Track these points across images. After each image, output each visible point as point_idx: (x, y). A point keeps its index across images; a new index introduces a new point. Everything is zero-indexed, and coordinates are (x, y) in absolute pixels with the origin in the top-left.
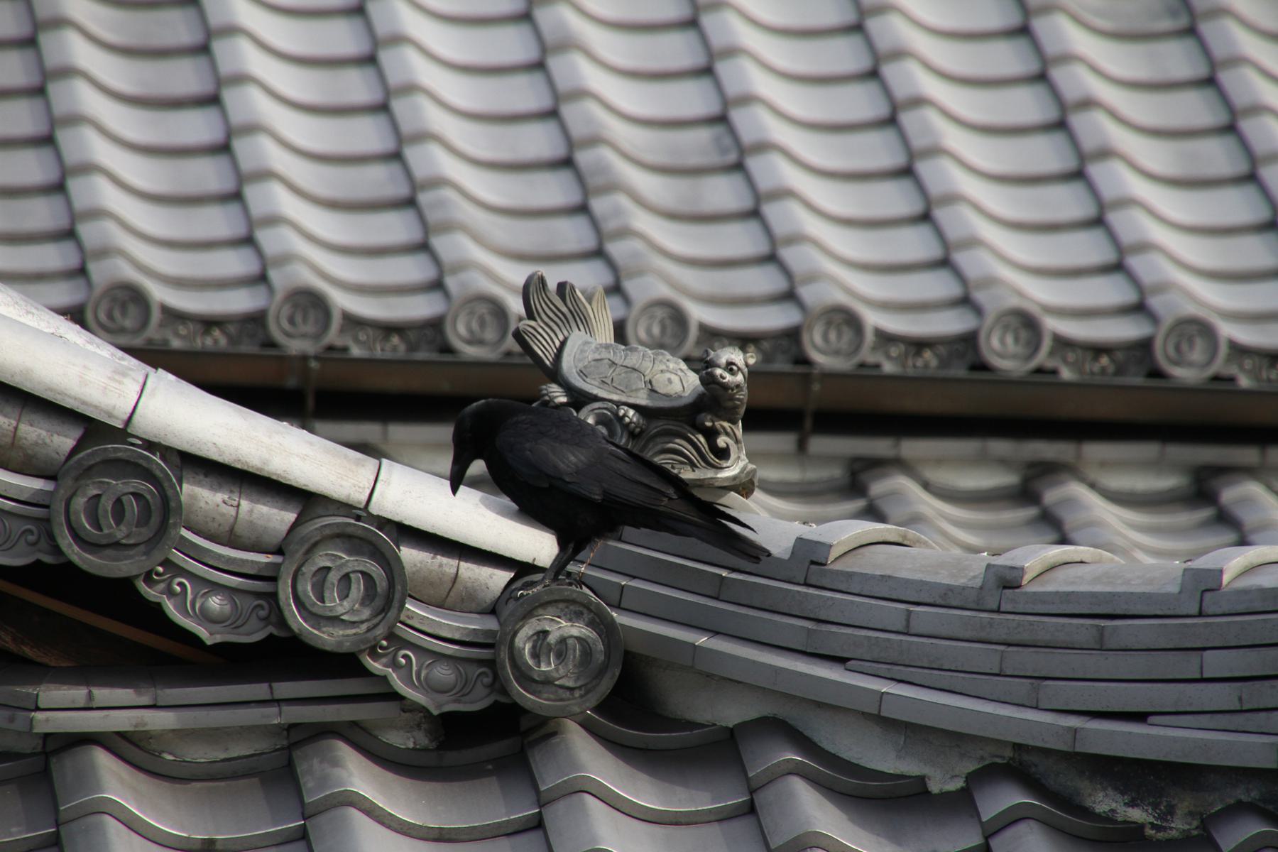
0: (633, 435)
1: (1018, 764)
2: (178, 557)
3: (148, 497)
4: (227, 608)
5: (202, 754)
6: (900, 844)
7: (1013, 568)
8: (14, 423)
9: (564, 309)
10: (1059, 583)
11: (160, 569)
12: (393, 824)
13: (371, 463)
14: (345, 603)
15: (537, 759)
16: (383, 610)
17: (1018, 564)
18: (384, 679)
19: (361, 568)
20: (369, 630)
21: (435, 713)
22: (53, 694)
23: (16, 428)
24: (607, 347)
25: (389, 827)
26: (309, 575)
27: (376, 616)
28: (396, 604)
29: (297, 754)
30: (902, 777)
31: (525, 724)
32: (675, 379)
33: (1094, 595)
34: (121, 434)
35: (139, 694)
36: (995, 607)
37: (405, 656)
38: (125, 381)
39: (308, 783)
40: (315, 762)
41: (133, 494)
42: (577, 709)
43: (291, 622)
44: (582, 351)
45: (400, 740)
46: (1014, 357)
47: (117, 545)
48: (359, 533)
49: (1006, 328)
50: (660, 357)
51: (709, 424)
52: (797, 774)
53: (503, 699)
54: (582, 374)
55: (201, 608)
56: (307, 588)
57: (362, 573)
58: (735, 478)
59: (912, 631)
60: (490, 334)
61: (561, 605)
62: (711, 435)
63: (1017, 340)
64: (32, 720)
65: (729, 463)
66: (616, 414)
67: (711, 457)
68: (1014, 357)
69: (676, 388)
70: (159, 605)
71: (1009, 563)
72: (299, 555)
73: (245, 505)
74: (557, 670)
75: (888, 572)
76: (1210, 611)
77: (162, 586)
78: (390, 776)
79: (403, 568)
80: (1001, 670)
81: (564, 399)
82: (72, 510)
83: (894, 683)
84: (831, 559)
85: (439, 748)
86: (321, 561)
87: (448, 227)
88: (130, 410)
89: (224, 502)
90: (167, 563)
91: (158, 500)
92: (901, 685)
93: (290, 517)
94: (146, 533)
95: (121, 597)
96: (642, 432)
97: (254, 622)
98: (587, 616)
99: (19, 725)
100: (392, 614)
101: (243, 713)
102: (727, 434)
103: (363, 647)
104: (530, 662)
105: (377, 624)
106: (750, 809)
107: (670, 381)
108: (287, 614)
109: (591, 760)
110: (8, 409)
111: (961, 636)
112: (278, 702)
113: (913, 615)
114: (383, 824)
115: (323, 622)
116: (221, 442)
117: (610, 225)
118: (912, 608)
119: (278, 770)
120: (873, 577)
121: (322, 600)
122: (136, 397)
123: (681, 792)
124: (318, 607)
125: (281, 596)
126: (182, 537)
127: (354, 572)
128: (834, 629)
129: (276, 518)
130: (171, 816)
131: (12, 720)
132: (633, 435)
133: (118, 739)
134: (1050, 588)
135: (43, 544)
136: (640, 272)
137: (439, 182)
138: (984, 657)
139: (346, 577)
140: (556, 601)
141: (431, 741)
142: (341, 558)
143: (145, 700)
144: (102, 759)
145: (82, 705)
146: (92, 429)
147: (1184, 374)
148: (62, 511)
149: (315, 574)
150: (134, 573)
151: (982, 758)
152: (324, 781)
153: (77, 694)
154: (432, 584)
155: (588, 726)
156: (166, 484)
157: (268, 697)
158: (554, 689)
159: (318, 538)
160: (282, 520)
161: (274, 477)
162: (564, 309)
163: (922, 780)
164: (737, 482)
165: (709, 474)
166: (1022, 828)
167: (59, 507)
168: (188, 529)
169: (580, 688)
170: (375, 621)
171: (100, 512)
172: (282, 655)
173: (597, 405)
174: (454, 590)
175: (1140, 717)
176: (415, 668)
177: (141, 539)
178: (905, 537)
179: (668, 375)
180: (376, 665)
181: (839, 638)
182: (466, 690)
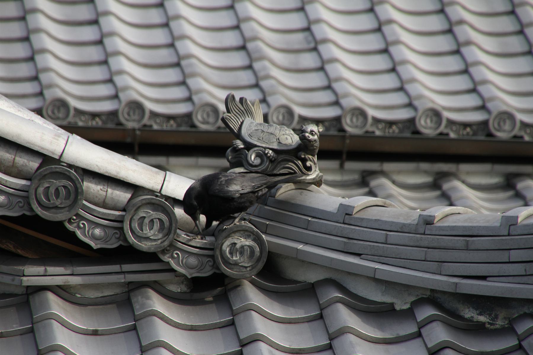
0: (271, 161)
1: (432, 297)
2: (82, 212)
3: (69, 187)
4: (103, 234)
5: (92, 294)
7: (430, 216)
8: (13, 157)
9: (242, 109)
10: (450, 222)
11: (75, 218)
12: (172, 323)
13: (162, 173)
14: (152, 231)
15: (232, 296)
17: (432, 214)
18: (168, 263)
19: (158, 217)
20: (161, 243)
21: (189, 277)
22: (30, 269)
23: (14, 159)
24: (261, 124)
25: (170, 325)
26: (136, 220)
28: (173, 232)
29: (132, 294)
30: (384, 303)
31: (227, 281)
32: (289, 138)
33: (464, 227)
34: (58, 161)
35: (66, 270)
36: (423, 232)
37: (176, 254)
38: (60, 139)
39: (136, 306)
40: (140, 298)
41: (63, 186)
42: (248, 275)
43: (129, 240)
44: (250, 126)
45: (175, 288)
46: (431, 128)
47: (56, 207)
48: (157, 202)
49: (427, 116)
50: (283, 129)
51: (303, 156)
53: (217, 271)
54: (250, 136)
55: (91, 234)
56: (135, 225)
57: (159, 219)
58: (314, 179)
59: (388, 242)
60: (211, 120)
61: (242, 232)
62: (304, 161)
63: (431, 121)
64: (21, 280)
65: (311, 173)
66: (264, 153)
68: (431, 128)
69: (289, 141)
70: (74, 232)
71: (429, 214)
72: (132, 212)
73: (110, 191)
74: (240, 259)
75: (378, 218)
76: (513, 234)
77: (75, 225)
81: (242, 146)
82: (38, 193)
83: (380, 264)
84: (354, 212)
85: (191, 292)
87: (194, 75)
88: (61, 151)
89: (101, 190)
90: (77, 215)
93: (128, 196)
94: (68, 202)
95: (58, 229)
96: (275, 160)
97: (113, 240)
98: (252, 237)
99: (16, 282)
100: (171, 236)
102: (311, 161)
103: (159, 250)
104: (229, 256)
107: (287, 138)
108: (127, 236)
109: (254, 296)
110: (11, 151)
113: (389, 236)
114: (168, 323)
115: (142, 240)
116: (99, 164)
117: (261, 74)
119: (124, 300)
120: (371, 220)
122: (64, 146)
123: (292, 310)
124: (140, 233)
125: (125, 229)
126: (84, 204)
128: (355, 242)
129: (123, 196)
131: (13, 280)
133: (58, 288)
135: (26, 207)
136: (274, 93)
137: (190, 56)
138: (419, 253)
141: (188, 289)
143: (68, 272)
144: (51, 297)
146: (46, 159)
147: (501, 135)
150: (64, 219)
152: (143, 305)
153: (40, 269)
155: (253, 282)
156: (77, 182)
157: (120, 271)
158: (238, 267)
159: (140, 205)
160: (125, 197)
161: (122, 179)
162: (242, 109)
163: (392, 304)
164: (315, 181)
166: (434, 324)
169: (249, 267)
171: (49, 194)
172: (125, 253)
173: (256, 149)
175: (483, 278)
176: (181, 259)
177: (66, 205)
178: (385, 203)
179: (286, 136)
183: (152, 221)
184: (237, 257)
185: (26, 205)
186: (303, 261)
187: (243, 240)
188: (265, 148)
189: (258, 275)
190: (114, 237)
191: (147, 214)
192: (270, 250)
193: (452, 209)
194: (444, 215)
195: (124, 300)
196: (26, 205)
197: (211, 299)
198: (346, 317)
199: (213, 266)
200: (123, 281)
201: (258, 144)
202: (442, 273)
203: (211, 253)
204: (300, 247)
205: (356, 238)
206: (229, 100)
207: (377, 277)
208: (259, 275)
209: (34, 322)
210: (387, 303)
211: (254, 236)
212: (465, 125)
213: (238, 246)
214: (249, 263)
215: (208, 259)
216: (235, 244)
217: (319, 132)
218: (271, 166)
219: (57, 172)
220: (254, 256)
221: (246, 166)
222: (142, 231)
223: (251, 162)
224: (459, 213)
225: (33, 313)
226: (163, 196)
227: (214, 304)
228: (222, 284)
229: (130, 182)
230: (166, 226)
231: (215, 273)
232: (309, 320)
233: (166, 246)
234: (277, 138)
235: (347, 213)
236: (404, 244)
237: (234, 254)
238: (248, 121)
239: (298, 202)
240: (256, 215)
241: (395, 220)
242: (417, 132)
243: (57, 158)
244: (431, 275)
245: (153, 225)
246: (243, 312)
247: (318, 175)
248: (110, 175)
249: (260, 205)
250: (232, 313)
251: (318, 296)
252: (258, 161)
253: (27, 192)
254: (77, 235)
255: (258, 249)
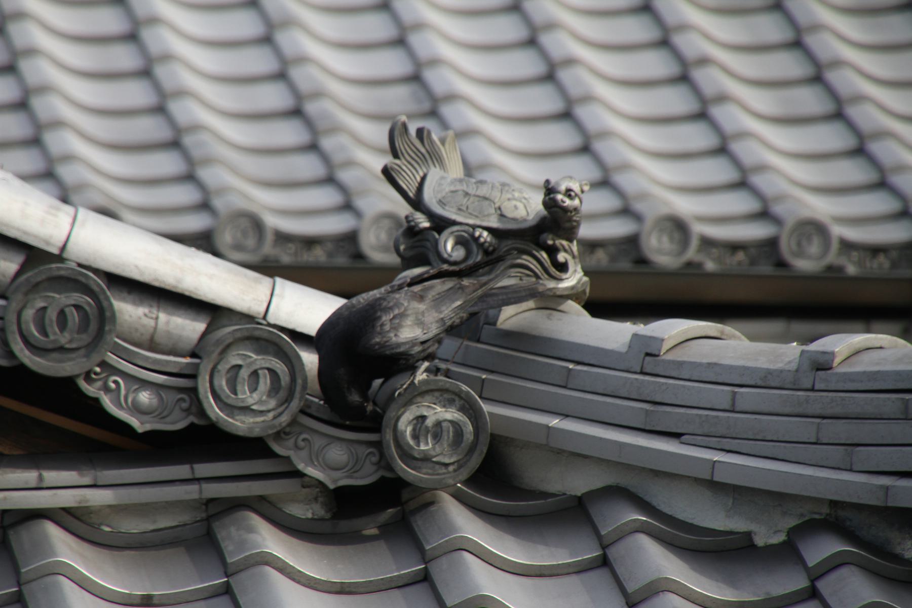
1: (835, 518)
2: (112, 359)
3: (87, 308)
4: (155, 401)
5: (134, 526)
7: (824, 353)
9: (423, 150)
11: (98, 369)
12: (302, 580)
13: (266, 281)
15: (419, 523)
16: (286, 401)
17: (828, 349)
20: (275, 418)
21: (332, 487)
24: (461, 181)
25: (298, 582)
26: (223, 372)
27: (282, 404)
29: (216, 525)
31: (405, 495)
33: (898, 373)
35: (82, 475)
39: (228, 547)
42: (451, 482)
44: (440, 185)
45: (301, 511)
47: (61, 349)
48: (265, 335)
51: (550, 242)
53: (388, 475)
54: (441, 203)
56: (222, 383)
57: (269, 369)
58: (573, 288)
59: (738, 409)
60: (251, 242)
61: (437, 394)
62: (552, 251)
65: (568, 275)
66: (472, 236)
67: (553, 270)
69: (521, 213)
70: (97, 400)
71: (821, 349)
72: (215, 356)
73: (163, 317)
74: (434, 448)
78: (294, 541)
80: (818, 439)
81: (426, 224)
83: (723, 453)
86: (234, 359)
87: (209, 161)
88: (64, 238)
89: (145, 315)
90: (103, 364)
92: (730, 455)
94: (86, 338)
95: (64, 395)
96: (494, 250)
97: (177, 414)
98: (458, 402)
101: (170, 488)
102: (566, 251)
103: (270, 432)
104: (412, 442)
106: (604, 562)
107: (516, 207)
108: (205, 405)
111: (780, 411)
112: (198, 480)
113: (738, 396)
114: (293, 580)
115: (236, 412)
117: (337, 158)
118: (737, 389)
119: (201, 535)
124: (231, 399)
125: (201, 390)
126: (116, 343)
127: (262, 368)
129: (190, 328)
133: (64, 514)
134: (859, 368)
137: (196, 128)
140: (432, 391)
141: (327, 512)
142: (250, 357)
143: (87, 480)
144: (53, 531)
145: (33, 485)
147: (804, 265)
150: (76, 372)
151: (802, 515)
152: (242, 545)
153: (29, 476)
155: (459, 497)
156: (102, 297)
157: (189, 476)
158: (431, 465)
159: (231, 340)
161: (187, 293)
162: (423, 150)
163: (748, 535)
165: (551, 284)
166: (844, 571)
178: (722, 332)
179: (514, 202)
181: (671, 418)
183: (255, 374)
184: (427, 444)
186: (560, 452)
187: (439, 409)
189: (468, 482)
190: (177, 408)
191: (244, 360)
192: (496, 432)
193: (868, 339)
194: (852, 351)
195: (201, 535)
197: (374, 531)
198: (656, 560)
199: (378, 463)
201: (459, 219)
202: (855, 468)
204: (555, 422)
205: (669, 402)
206: (396, 133)
207: (715, 479)
209: (22, 581)
211: (462, 402)
212: (734, 247)
214: (451, 456)
215: (371, 450)
216: (423, 418)
220: (462, 442)
222: (236, 394)
223: (445, 256)
224: (881, 348)
225: (20, 563)
226: (269, 325)
230: (283, 383)
233: (284, 425)
234: (497, 205)
235: (649, 351)
236: (771, 410)
237: (422, 439)
238: (434, 174)
239: (546, 334)
240: (459, 361)
242: (642, 261)
243: (56, 251)
247: (580, 280)
249: (466, 343)
251: (595, 520)
252: (459, 254)
254: (104, 404)
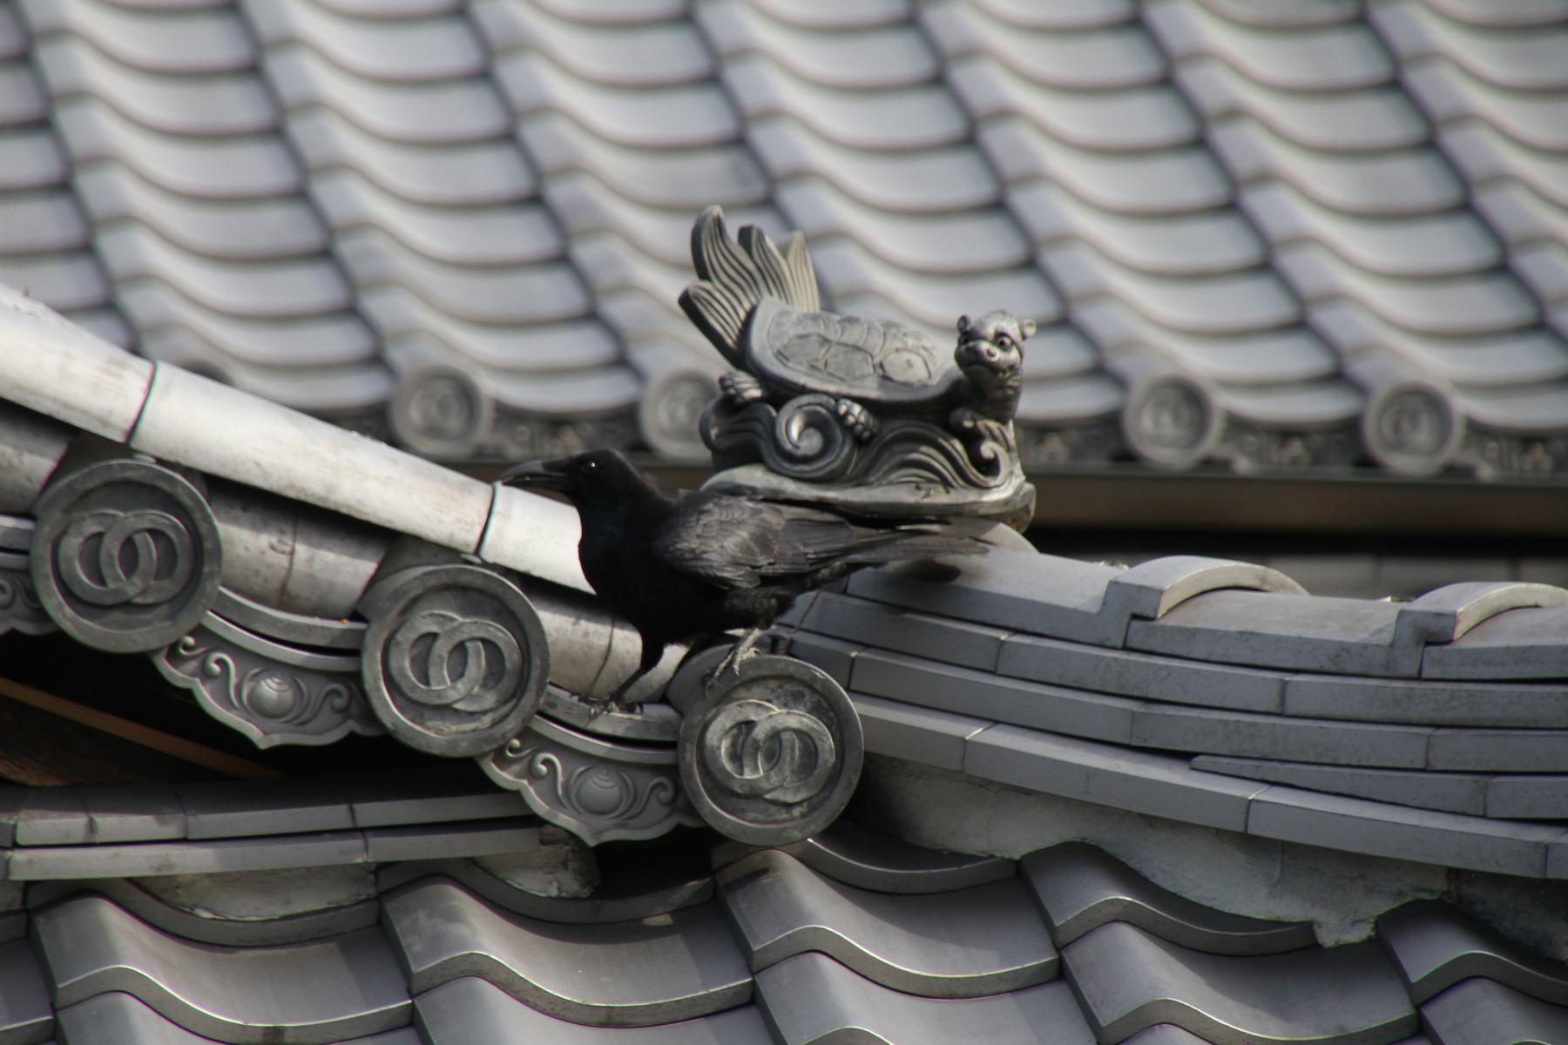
0: (860, 442)
1: (1457, 898)
2: (215, 622)
3: (172, 535)
4: (288, 696)
5: (252, 909)
6: (1287, 1019)
7: (1439, 615)
9: (750, 265)
11: (190, 640)
12: (539, 1002)
13: (481, 490)
14: (459, 685)
15: (742, 906)
16: (513, 695)
17: (1447, 608)
18: (516, 795)
20: (494, 724)
21: (592, 843)
22: (37, 824)
24: (814, 318)
25: (534, 1007)
26: (406, 646)
27: (505, 702)
28: (533, 685)
29: (391, 906)
31: (718, 857)
34: (125, 449)
35: (163, 823)
36: (1413, 672)
37: (546, 762)
39: (414, 947)
40: (421, 915)
41: (150, 531)
42: (797, 835)
44: (779, 324)
45: (539, 884)
47: (127, 605)
48: (478, 582)
51: (968, 424)
52: (1127, 922)
53: (689, 822)
54: (781, 356)
55: (250, 697)
56: (403, 664)
57: (484, 641)
58: (1007, 502)
59: (1290, 711)
60: (454, 423)
61: (772, 684)
62: (972, 440)
64: (7, 862)
66: (835, 413)
67: (972, 472)
69: (918, 373)
70: (188, 694)
72: (392, 616)
73: (302, 550)
74: (767, 778)
75: (1250, 627)
77: (192, 665)
78: (528, 936)
79: (542, 632)
80: (1428, 763)
81: (755, 393)
83: (1265, 787)
84: (1162, 610)
85: (593, 897)
86: (424, 623)
87: (383, 283)
88: (132, 416)
89: (272, 547)
90: (200, 631)
91: (187, 539)
94: (169, 587)
95: (133, 684)
96: (872, 437)
97: (327, 716)
98: (809, 698)
100: (528, 700)
102: (995, 439)
103: (486, 748)
104: (729, 767)
105: (507, 715)
106: (1059, 973)
107: (909, 364)
108: (375, 703)
111: (1363, 715)
112: (362, 831)
114: (525, 1002)
115: (427, 714)
116: (266, 460)
117: (604, 278)
118: (1288, 677)
119: (369, 925)
120: (1227, 634)
121: (426, 680)
123: (953, 952)
124: (419, 691)
125: (368, 676)
126: (221, 594)
128: (1171, 710)
129: (349, 569)
130: (217, 997)
132: (860, 442)
133: (133, 888)
134: (1497, 642)
135: (20, 606)
137: (362, 226)
138: (1404, 746)
139: (460, 648)
141: (583, 886)
142: (452, 619)
143: (171, 831)
144: (112, 917)
145: (80, 840)
146: (79, 443)
147: (1405, 464)
148: (47, 555)
149: (414, 644)
150: (154, 645)
151: (1400, 894)
152: (437, 942)
153: (72, 824)
154: (573, 661)
155: (810, 861)
156: (197, 516)
157: (347, 824)
158: (763, 806)
161: (344, 510)
162: (750, 265)
163: (1308, 928)
164: (1009, 508)
166: (1473, 990)
167: (43, 551)
168: (224, 585)
169: (800, 803)
170: (505, 709)
171: (103, 558)
172: (367, 763)
173: (805, 399)
174: (606, 669)
178: (1264, 579)
179: (906, 356)
180: (505, 775)
181: (1176, 727)
182: (635, 810)
184: (756, 769)
185: (19, 599)
186: (984, 784)
187: (776, 710)
188: (838, 397)
189: (827, 835)
190: (326, 707)
191: (442, 624)
193: (1513, 592)
195: (369, 925)
196: (19, 599)
197: (664, 920)
198: (1148, 970)
200: (360, 860)
202: (1490, 813)
203: (666, 757)
205: (1172, 699)
206: (705, 236)
207: (1253, 831)
208: (830, 834)
209: (58, 1006)
210: (1290, 924)
211: (816, 697)
212: (1285, 433)
213: (760, 733)
214: (798, 790)
216: (750, 725)
217: (1024, 337)
218: (860, 459)
219: (128, 483)
221: (770, 461)
222: (427, 683)
223: (788, 447)
224: (1536, 606)
227: (678, 936)
228: (700, 867)
229: (373, 519)
230: (508, 665)
231: (679, 828)
232: (1016, 985)
234: (877, 360)
235: (1137, 611)
236: (1347, 712)
237: (747, 761)
238: (769, 306)
240: (812, 628)
241: (1311, 634)
242: (1127, 456)
243: (118, 437)
244: (1452, 818)
245: (465, 664)
246: (786, 958)
247: (1020, 488)
248: (302, 497)
250: (749, 967)
252: (812, 443)
253: (25, 552)
255: (828, 742)
